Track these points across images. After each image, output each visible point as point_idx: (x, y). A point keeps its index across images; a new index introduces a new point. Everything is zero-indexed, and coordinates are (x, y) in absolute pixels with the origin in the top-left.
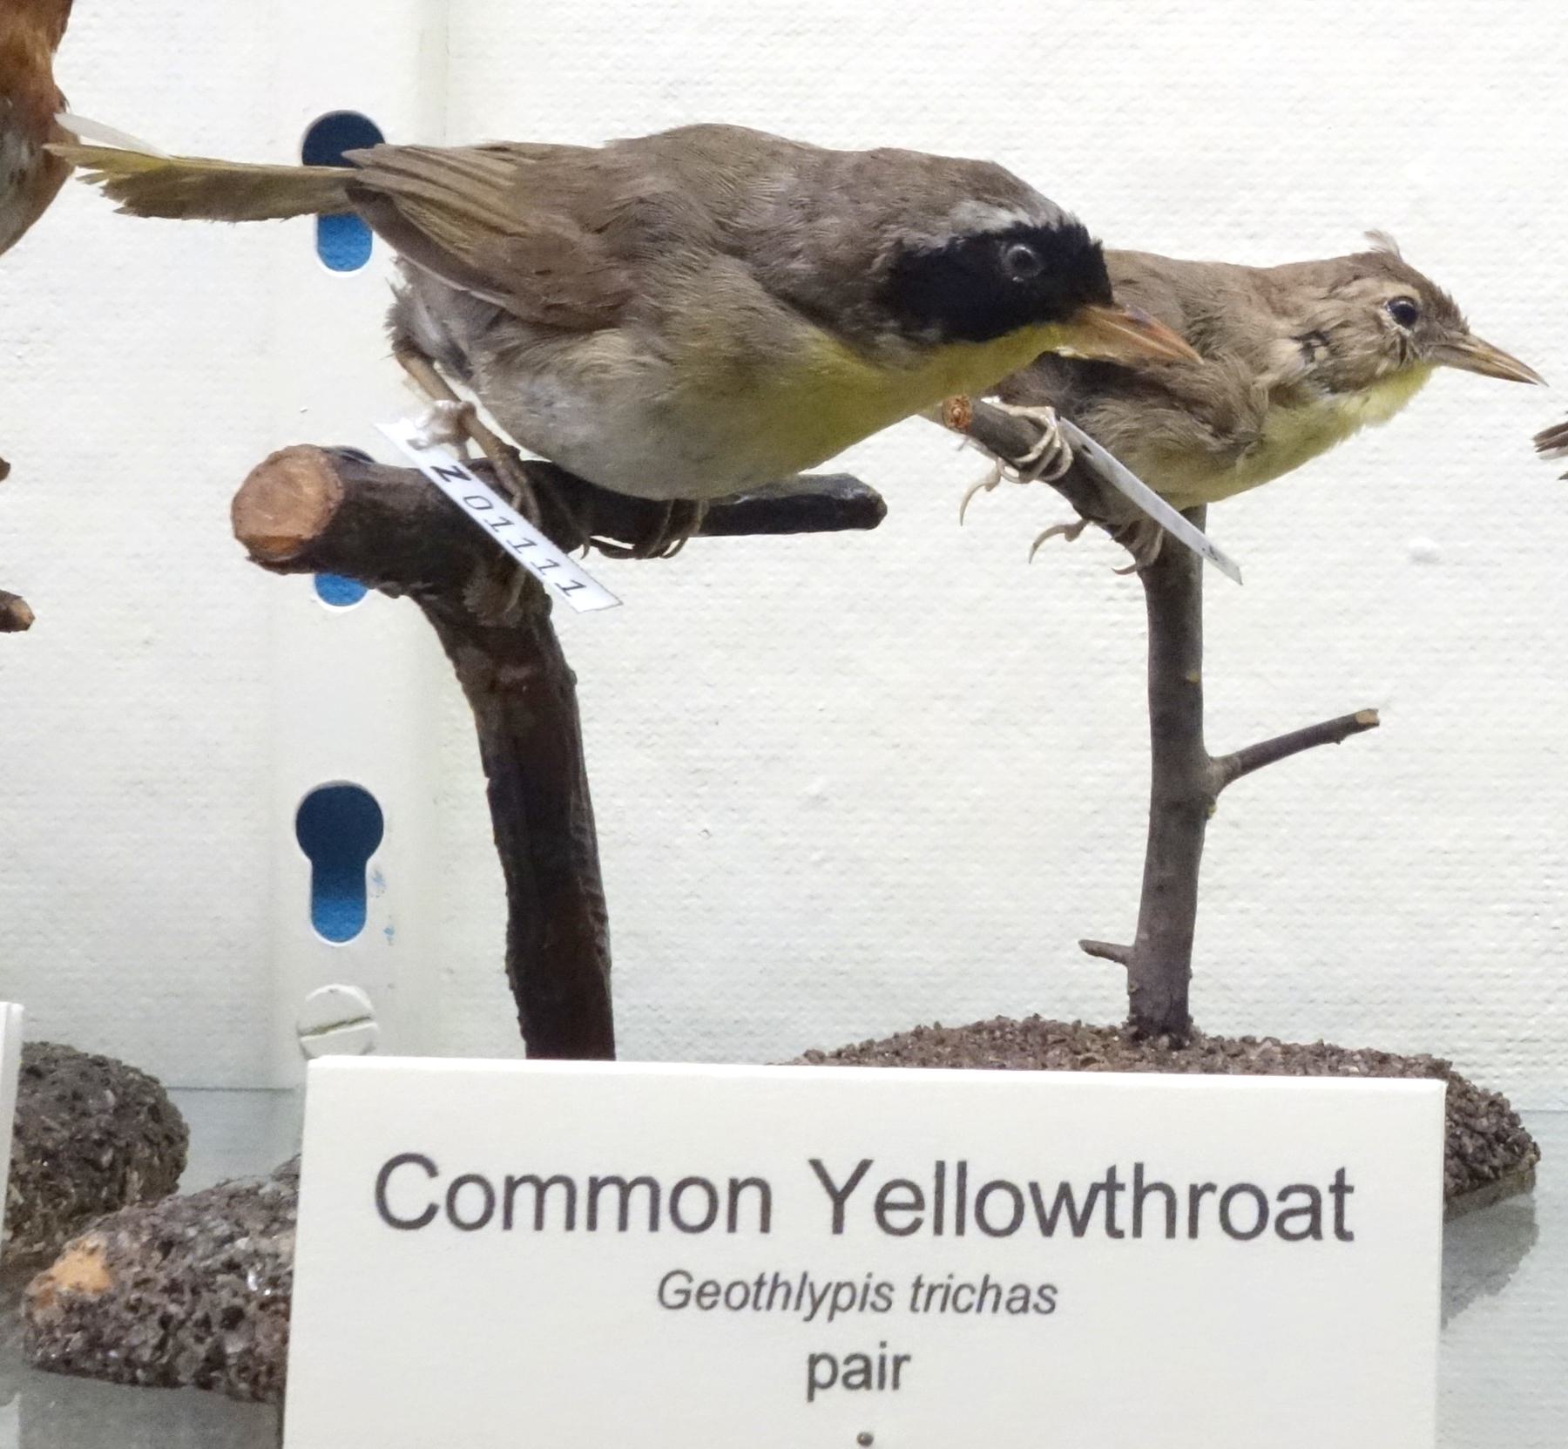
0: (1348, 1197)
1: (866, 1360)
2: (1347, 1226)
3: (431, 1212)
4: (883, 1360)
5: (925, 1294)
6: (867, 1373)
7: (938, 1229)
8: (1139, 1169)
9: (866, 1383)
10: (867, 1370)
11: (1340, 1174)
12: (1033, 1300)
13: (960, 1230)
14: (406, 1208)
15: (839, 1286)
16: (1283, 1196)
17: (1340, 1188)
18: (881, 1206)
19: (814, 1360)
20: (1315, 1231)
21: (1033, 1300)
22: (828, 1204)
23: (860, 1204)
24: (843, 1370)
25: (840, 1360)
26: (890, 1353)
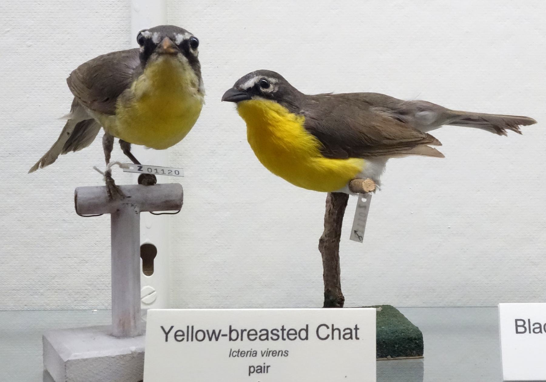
0: (358, 331)
1: (261, 367)
2: (358, 337)
3: (328, 336)
4: (264, 367)
5: (268, 353)
6: (261, 369)
7: (188, 340)
8: (333, 325)
9: (261, 372)
10: (261, 369)
11: (356, 326)
12: (286, 353)
13: (192, 340)
14: (323, 335)
15: (270, 352)
16: (260, 331)
17: (356, 329)
18: (176, 336)
19: (250, 367)
20: (351, 338)
21: (286, 353)
22: (165, 335)
23: (171, 335)
24: (256, 369)
25: (255, 367)
26: (266, 365)
